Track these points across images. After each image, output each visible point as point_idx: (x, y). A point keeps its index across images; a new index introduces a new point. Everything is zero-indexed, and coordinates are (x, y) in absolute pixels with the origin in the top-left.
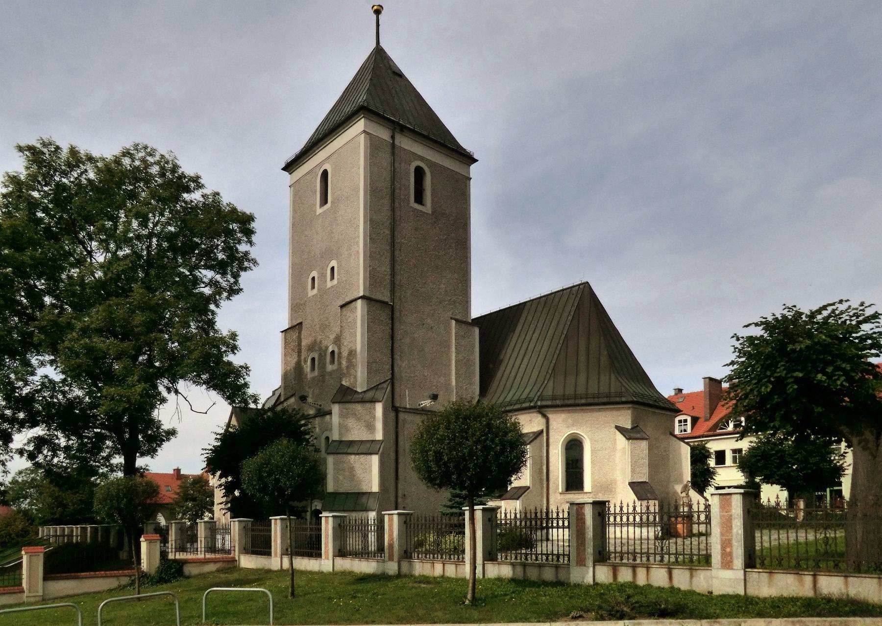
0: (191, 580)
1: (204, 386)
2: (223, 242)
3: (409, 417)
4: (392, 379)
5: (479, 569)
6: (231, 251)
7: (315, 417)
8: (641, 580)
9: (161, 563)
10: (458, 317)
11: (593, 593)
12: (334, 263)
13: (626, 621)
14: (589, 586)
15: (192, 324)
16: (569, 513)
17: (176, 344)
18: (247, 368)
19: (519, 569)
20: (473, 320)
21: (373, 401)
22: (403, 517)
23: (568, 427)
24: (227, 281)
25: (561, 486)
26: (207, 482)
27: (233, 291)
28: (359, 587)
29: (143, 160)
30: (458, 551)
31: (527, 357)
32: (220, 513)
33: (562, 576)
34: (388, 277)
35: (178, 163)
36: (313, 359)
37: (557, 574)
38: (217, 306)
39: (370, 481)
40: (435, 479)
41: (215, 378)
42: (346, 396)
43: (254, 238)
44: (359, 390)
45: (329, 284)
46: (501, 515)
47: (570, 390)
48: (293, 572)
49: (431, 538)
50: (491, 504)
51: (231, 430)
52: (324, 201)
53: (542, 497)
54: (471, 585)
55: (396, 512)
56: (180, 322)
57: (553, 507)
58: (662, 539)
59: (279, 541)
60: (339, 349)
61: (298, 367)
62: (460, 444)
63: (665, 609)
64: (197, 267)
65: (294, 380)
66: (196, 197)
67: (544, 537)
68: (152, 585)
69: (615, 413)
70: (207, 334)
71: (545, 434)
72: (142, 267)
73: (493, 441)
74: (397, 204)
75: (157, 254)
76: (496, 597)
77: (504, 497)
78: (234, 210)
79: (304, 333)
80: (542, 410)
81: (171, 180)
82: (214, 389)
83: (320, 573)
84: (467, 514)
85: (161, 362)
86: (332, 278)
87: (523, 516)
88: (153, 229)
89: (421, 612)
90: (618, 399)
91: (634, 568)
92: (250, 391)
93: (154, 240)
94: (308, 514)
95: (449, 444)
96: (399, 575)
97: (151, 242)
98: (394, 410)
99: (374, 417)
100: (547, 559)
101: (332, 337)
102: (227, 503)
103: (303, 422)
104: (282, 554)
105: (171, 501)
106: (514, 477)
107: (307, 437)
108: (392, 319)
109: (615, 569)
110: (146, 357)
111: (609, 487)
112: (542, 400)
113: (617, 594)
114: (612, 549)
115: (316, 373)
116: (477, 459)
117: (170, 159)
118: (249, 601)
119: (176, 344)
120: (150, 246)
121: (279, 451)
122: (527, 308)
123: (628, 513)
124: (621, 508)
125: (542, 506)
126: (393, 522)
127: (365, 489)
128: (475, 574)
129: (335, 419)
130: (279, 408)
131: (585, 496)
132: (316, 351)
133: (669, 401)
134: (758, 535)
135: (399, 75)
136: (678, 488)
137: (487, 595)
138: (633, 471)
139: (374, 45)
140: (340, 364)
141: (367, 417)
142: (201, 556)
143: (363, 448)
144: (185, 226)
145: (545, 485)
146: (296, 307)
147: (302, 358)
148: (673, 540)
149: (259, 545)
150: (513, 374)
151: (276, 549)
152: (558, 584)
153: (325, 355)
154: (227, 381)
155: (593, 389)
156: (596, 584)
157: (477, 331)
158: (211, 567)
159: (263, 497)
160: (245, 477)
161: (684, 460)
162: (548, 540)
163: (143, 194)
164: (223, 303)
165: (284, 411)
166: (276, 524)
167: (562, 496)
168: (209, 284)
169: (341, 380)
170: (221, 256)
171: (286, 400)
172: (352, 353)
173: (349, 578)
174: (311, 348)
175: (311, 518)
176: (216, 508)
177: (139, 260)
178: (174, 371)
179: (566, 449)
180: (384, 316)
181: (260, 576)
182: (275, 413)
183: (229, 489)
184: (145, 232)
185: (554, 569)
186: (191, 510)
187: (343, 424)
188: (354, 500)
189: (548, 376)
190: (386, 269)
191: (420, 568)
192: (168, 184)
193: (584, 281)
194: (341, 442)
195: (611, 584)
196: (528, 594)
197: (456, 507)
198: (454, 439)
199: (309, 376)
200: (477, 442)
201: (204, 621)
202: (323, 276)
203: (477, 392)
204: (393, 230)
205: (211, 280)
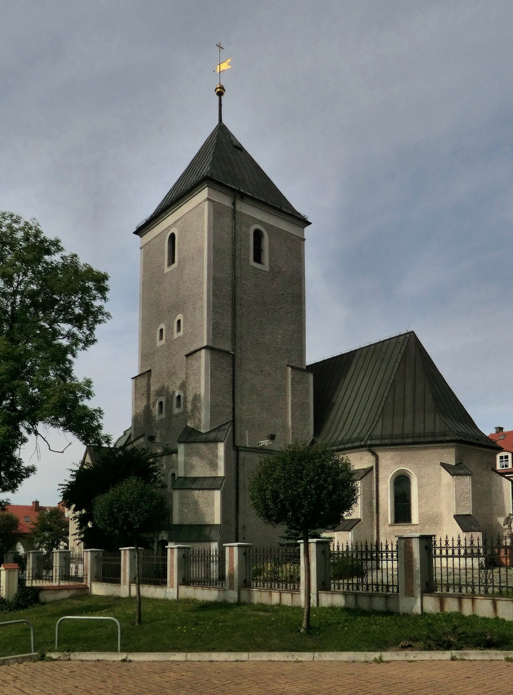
0: (47, 606)
1: (61, 428)
2: (80, 298)
3: (249, 456)
4: (233, 421)
5: (313, 598)
6: (87, 307)
7: (162, 455)
8: (467, 611)
9: (19, 591)
10: (293, 364)
11: (421, 622)
12: (180, 317)
13: (453, 651)
14: (417, 616)
15: (51, 372)
16: (397, 546)
17: (37, 390)
18: (100, 411)
19: (351, 599)
20: (307, 367)
21: (216, 441)
22: (243, 550)
24: (83, 332)
25: (390, 519)
26: (63, 514)
27: (89, 342)
28: (201, 614)
29: (10, 227)
30: (294, 579)
31: (358, 400)
32: (74, 543)
33: (392, 606)
34: (230, 329)
35: (41, 229)
36: (161, 403)
37: (387, 603)
38: (74, 356)
39: (213, 514)
40: (273, 515)
41: (71, 421)
42: (190, 436)
43: (108, 295)
44: (203, 431)
45: (176, 335)
46: (334, 548)
47: (397, 431)
48: (140, 600)
49: (269, 567)
50: (325, 535)
51: (85, 467)
52: (172, 260)
53: (373, 528)
54: (305, 614)
55: (236, 544)
56: (40, 370)
57: (382, 540)
58: (487, 568)
59: (128, 571)
60: (185, 393)
61: (147, 410)
62: (296, 483)
63: (490, 640)
64: (55, 321)
65: (143, 422)
66: (56, 258)
67: (374, 566)
68: (10, 610)
69: (441, 451)
70: (65, 380)
71: (374, 471)
72: (6, 321)
73: (325, 480)
74: (237, 263)
75: (20, 310)
76: (329, 625)
77: (336, 529)
78: (90, 270)
79: (152, 380)
80: (371, 449)
81: (34, 244)
82: (70, 431)
83: (166, 600)
84: (302, 547)
85: (23, 406)
86: (179, 330)
87: (354, 548)
88: (17, 287)
89: (259, 640)
90: (442, 438)
91: (460, 599)
92: (103, 432)
93: (18, 297)
94: (156, 544)
95: (285, 483)
96: (239, 603)
97: (15, 299)
98: (235, 450)
99: (217, 456)
100: (377, 588)
101: (179, 383)
102: (80, 534)
103: (151, 460)
104: (131, 583)
105: (30, 531)
106: (346, 513)
107: (155, 474)
108: (233, 367)
109: (442, 600)
110: (8, 401)
111: (434, 519)
112: (371, 440)
113: (445, 624)
114: (438, 577)
115: (163, 416)
116: (311, 498)
117: (33, 225)
118: (99, 627)
119: (37, 390)
120: (14, 303)
121: (128, 488)
122: (358, 355)
123: (453, 547)
124: (447, 542)
125: (372, 537)
126: (233, 554)
127: (208, 521)
128: (309, 603)
129: (181, 458)
130: (129, 447)
131: (413, 528)
132: (163, 395)
133: (491, 440)
135: (239, 148)
136: (501, 520)
137: (321, 623)
138: (458, 505)
139: (217, 122)
140: (185, 407)
141: (210, 456)
142: (55, 584)
143: (205, 484)
144: (46, 285)
145: (375, 518)
146: (146, 355)
147: (151, 402)
148: (496, 570)
149: (110, 574)
150: (347, 410)
151: (125, 577)
152: (388, 613)
153: (172, 398)
154: (82, 423)
155: (419, 429)
156: (424, 614)
158: (65, 594)
159: (113, 531)
160: (96, 513)
161: (505, 494)
162: (378, 568)
163: (9, 257)
164: (80, 353)
165: (134, 450)
166: (125, 554)
167: (391, 527)
168: (67, 336)
169: (186, 422)
170: (78, 311)
171: (134, 441)
172: (196, 398)
173: (192, 605)
174: (159, 393)
175: (158, 550)
176: (71, 538)
177: (5, 315)
178: (34, 413)
180: (226, 363)
181: (109, 603)
182: (125, 452)
183: (83, 521)
184: (10, 290)
185: (384, 599)
186: (47, 539)
187: (190, 463)
188: (199, 532)
189: (377, 418)
190: (227, 321)
191: (259, 596)
192: (32, 248)
193: (410, 330)
194: (186, 478)
195: (438, 614)
196: (360, 623)
197: (292, 539)
198: (290, 479)
199: (157, 419)
200: (310, 482)
201: (56, 648)
202: (170, 328)
203: (312, 432)
205: (68, 333)
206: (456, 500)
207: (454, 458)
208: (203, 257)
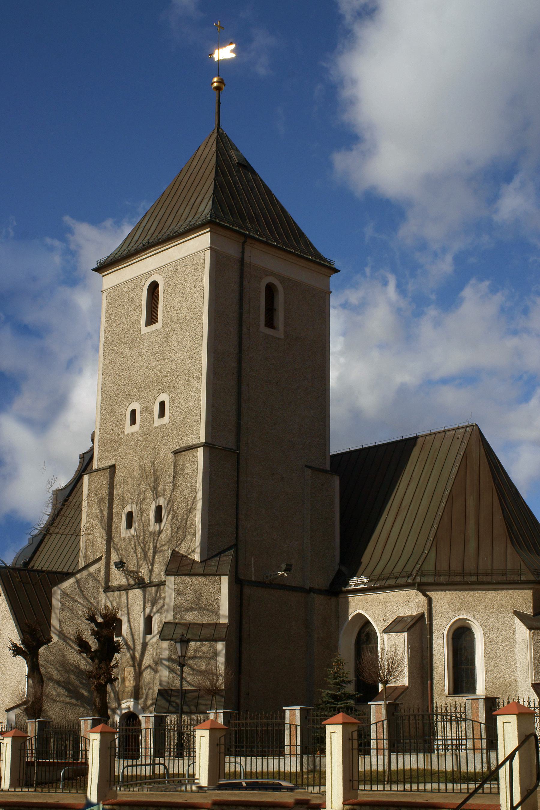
23: (455, 610)
52: (152, 319)
74: (245, 330)
90: (516, 578)
108: (238, 472)
112: (422, 575)
134: (183, 716)
157: (336, 481)
179: (453, 638)
193: (473, 422)
202: (148, 410)
204: (240, 361)
206: (535, 663)
207: (532, 605)
208: (202, 324)
